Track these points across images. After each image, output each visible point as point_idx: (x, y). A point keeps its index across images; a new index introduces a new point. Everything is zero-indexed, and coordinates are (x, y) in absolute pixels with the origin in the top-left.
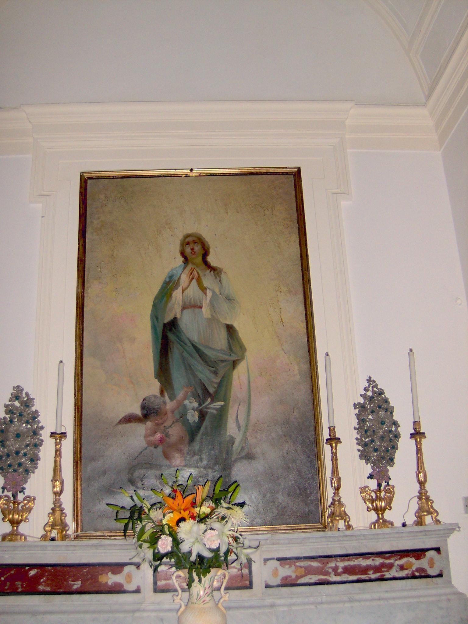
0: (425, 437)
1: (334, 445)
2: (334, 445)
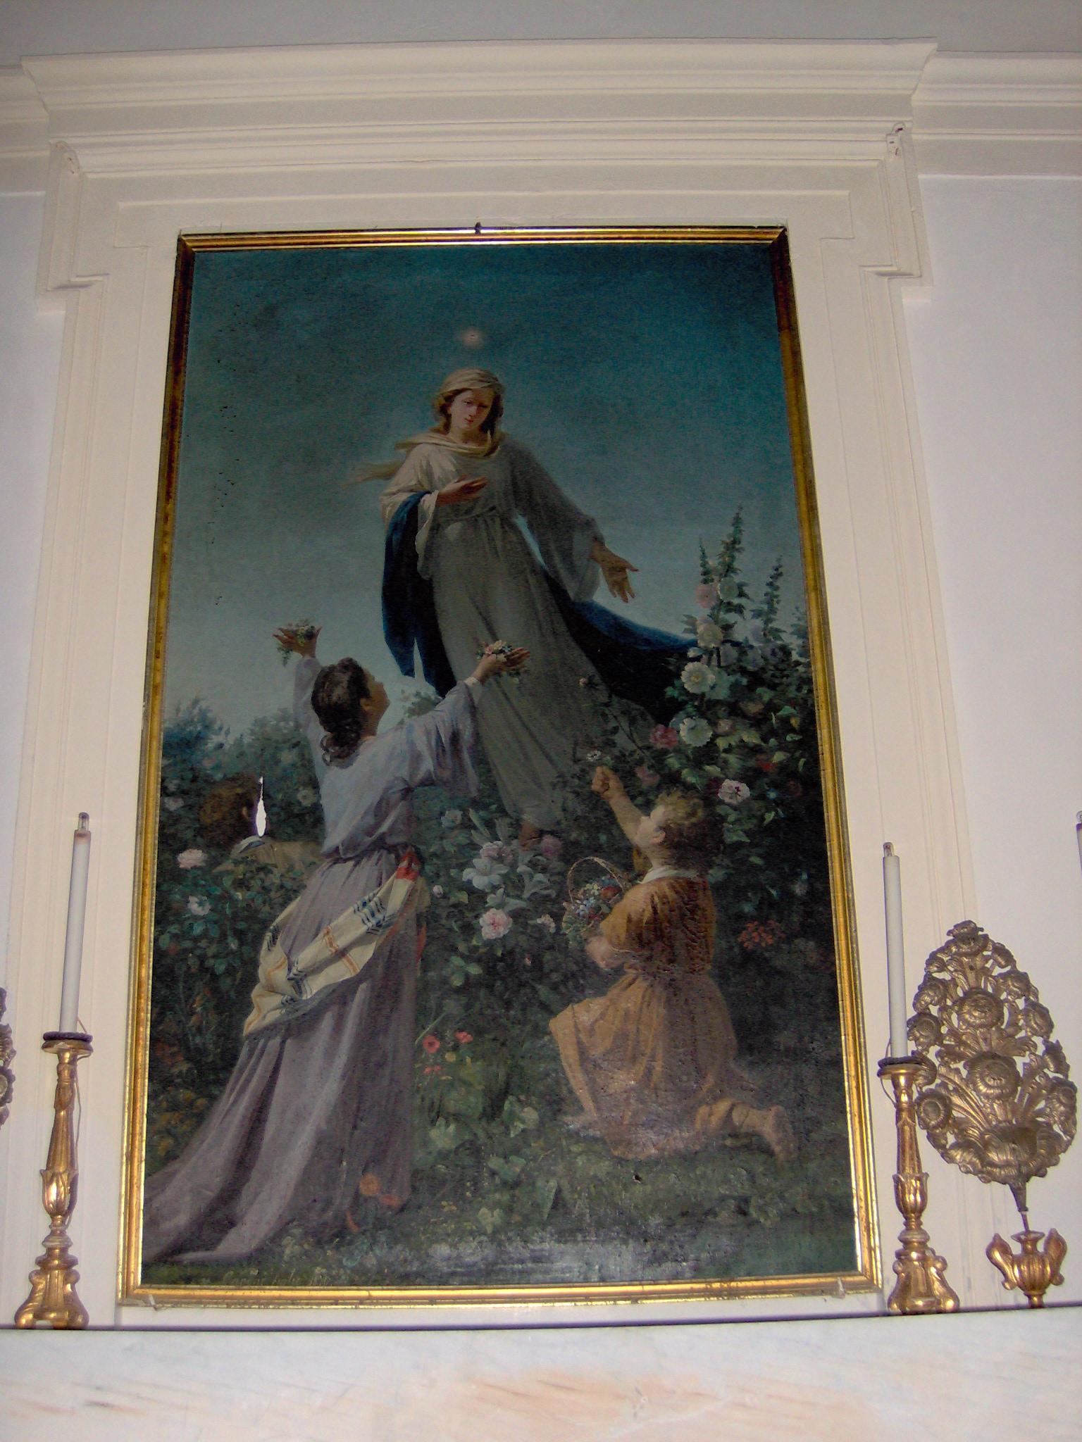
0: (90, 1050)
1: (902, 1080)
2: (902, 1080)
